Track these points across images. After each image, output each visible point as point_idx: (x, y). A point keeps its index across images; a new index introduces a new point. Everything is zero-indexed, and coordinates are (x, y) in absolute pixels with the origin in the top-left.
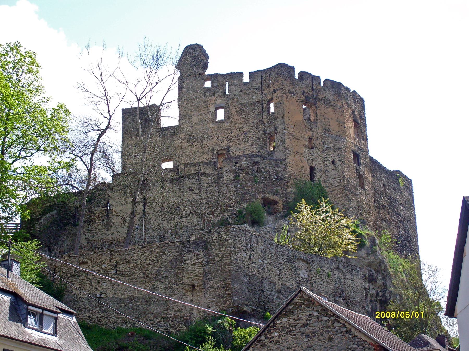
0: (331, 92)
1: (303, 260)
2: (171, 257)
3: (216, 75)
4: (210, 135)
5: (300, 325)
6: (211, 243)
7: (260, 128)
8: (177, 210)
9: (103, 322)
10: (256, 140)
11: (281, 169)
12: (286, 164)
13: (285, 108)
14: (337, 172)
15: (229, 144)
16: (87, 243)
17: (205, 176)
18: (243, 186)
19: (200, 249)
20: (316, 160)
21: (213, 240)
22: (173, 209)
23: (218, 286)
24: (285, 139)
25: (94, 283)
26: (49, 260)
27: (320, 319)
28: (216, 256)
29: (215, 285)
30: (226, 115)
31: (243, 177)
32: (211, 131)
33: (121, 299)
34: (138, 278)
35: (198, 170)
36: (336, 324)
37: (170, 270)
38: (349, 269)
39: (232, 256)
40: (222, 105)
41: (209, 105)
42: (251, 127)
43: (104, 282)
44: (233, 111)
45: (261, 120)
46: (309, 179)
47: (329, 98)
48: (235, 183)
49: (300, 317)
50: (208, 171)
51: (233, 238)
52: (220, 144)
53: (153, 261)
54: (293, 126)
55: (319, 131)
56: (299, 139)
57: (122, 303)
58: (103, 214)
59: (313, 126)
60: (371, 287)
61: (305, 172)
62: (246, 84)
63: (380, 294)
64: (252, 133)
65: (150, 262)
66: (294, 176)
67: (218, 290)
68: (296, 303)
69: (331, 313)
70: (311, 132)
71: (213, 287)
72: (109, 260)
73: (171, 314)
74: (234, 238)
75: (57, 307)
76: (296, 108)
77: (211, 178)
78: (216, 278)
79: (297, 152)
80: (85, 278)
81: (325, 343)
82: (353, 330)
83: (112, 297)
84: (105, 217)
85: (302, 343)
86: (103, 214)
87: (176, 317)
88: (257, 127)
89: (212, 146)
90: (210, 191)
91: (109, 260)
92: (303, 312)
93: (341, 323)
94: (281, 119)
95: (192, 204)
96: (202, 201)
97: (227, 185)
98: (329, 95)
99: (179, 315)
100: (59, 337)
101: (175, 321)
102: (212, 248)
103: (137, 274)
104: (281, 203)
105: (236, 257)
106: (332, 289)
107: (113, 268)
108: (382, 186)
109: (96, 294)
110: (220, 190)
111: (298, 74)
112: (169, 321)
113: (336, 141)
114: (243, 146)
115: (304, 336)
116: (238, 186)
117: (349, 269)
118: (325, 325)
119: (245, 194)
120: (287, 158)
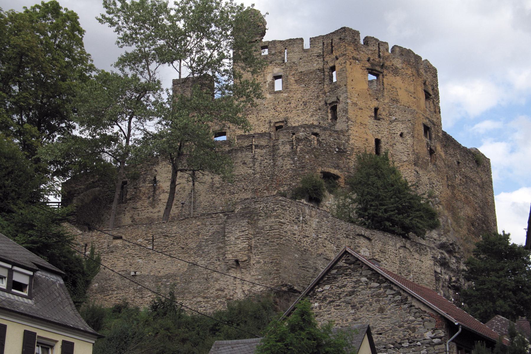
0: (400, 60)
1: (364, 236)
2: (213, 229)
3: (274, 42)
4: (266, 106)
5: (345, 293)
6: (257, 214)
7: (321, 98)
8: (228, 185)
9: (136, 303)
10: (316, 110)
11: (343, 141)
12: (349, 136)
13: (348, 75)
14: (405, 146)
15: (287, 116)
16: (132, 221)
17: (259, 148)
18: (301, 158)
19: (245, 221)
20: (382, 132)
21: (259, 210)
22: (224, 184)
23: (265, 262)
24: (347, 109)
25: (128, 259)
26: (80, 234)
27: (369, 286)
28: (263, 228)
29: (261, 260)
30: (284, 84)
31: (301, 149)
32: (267, 102)
33: (157, 277)
34: (176, 253)
35: (251, 142)
36: (389, 292)
37: (212, 244)
38: (418, 249)
39: (281, 228)
40: (280, 74)
41: (266, 75)
42: (311, 97)
43: (140, 259)
44: (292, 80)
45: (322, 90)
46: (375, 153)
47: (398, 66)
48: (292, 156)
49: (345, 283)
50: (262, 143)
51: (282, 209)
52: (277, 116)
53: (193, 234)
54: (356, 95)
55: (386, 101)
56: (364, 109)
57: (158, 282)
58: (149, 190)
59: (379, 96)
60: (443, 271)
61: (370, 145)
62: (306, 51)
63: (454, 279)
64: (312, 104)
65: (189, 236)
66: (358, 149)
67: (265, 266)
68: (341, 267)
69: (382, 278)
70: (376, 102)
71: (258, 262)
72: (146, 234)
73: (213, 293)
74: (284, 208)
75: (35, 264)
76: (361, 75)
77: (266, 150)
78: (263, 252)
79: (361, 123)
80: (118, 254)
81: (375, 315)
82: (409, 298)
83: (147, 275)
84: (152, 193)
85: (347, 315)
86: (149, 190)
87: (218, 297)
88: (318, 97)
89: (268, 117)
90: (264, 165)
91: (146, 234)
92: (349, 278)
93: (395, 290)
94: (344, 87)
95: (245, 179)
96: (255, 175)
97: (283, 157)
98: (398, 63)
99: (220, 295)
100: (36, 300)
101: (216, 301)
102: (259, 220)
103: (176, 249)
104: (343, 178)
105: (285, 230)
106: (397, 270)
107: (150, 243)
108: (456, 163)
109: (130, 272)
110: (275, 164)
111: (364, 40)
112: (209, 301)
113: (405, 112)
114: (302, 118)
115: (350, 307)
116: (296, 159)
117: (418, 249)
118: (375, 293)
119: (303, 168)
120: (350, 129)
